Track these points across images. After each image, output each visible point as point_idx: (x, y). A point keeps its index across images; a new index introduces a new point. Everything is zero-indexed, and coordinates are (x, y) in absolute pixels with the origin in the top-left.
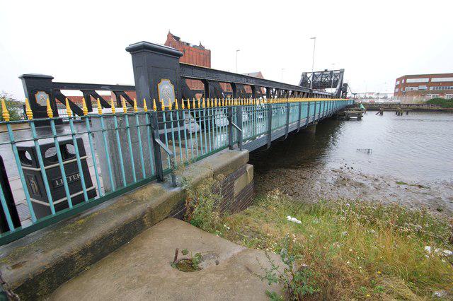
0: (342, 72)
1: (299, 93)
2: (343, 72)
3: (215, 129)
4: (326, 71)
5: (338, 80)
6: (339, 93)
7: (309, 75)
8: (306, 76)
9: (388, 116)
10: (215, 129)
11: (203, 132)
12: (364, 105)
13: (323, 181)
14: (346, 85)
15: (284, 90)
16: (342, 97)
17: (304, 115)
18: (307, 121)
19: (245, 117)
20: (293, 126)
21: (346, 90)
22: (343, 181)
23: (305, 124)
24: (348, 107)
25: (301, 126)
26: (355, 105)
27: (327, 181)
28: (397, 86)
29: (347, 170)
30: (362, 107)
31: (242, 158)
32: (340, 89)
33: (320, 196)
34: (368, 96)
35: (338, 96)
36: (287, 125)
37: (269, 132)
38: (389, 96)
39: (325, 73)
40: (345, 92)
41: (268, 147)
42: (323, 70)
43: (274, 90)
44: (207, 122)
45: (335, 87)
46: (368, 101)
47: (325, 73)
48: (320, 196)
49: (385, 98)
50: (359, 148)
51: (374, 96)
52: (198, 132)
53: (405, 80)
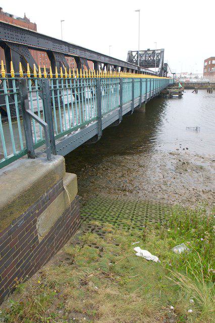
0: (162, 52)
1: (115, 67)
2: (163, 52)
3: (84, 101)
4: (149, 50)
5: (159, 60)
6: (161, 72)
7: (134, 54)
8: (132, 54)
9: (202, 93)
10: (84, 101)
11: (78, 102)
12: (181, 84)
13: (163, 167)
14: (166, 65)
15: (113, 64)
16: (164, 76)
17: (127, 97)
18: (140, 100)
19: (68, 97)
20: (127, 109)
21: (166, 69)
22: (183, 166)
23: (129, 110)
24: (170, 86)
25: (135, 106)
26: (175, 84)
27: (167, 167)
28: (205, 67)
29: (184, 152)
30: (180, 86)
31: (57, 167)
32: (162, 68)
33: (164, 187)
34: (183, 76)
35: (160, 75)
36: (121, 106)
37: (99, 118)
38: (200, 77)
39: (148, 52)
40: (166, 71)
41: (99, 138)
42: (147, 50)
43: (103, 65)
44: (81, 96)
45: (158, 66)
46: (184, 80)
47: (148, 52)
48: (164, 187)
49: (196, 78)
50: (189, 126)
51: (188, 76)
52: (74, 103)
53: (211, 62)
